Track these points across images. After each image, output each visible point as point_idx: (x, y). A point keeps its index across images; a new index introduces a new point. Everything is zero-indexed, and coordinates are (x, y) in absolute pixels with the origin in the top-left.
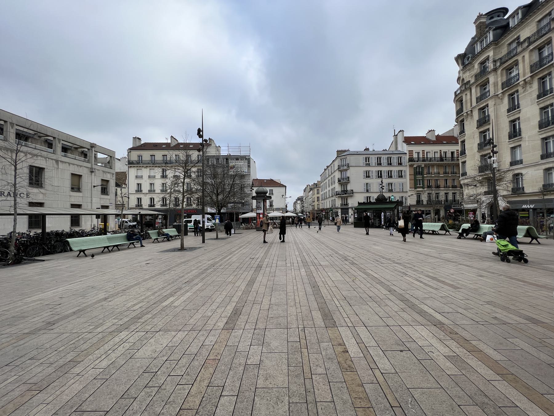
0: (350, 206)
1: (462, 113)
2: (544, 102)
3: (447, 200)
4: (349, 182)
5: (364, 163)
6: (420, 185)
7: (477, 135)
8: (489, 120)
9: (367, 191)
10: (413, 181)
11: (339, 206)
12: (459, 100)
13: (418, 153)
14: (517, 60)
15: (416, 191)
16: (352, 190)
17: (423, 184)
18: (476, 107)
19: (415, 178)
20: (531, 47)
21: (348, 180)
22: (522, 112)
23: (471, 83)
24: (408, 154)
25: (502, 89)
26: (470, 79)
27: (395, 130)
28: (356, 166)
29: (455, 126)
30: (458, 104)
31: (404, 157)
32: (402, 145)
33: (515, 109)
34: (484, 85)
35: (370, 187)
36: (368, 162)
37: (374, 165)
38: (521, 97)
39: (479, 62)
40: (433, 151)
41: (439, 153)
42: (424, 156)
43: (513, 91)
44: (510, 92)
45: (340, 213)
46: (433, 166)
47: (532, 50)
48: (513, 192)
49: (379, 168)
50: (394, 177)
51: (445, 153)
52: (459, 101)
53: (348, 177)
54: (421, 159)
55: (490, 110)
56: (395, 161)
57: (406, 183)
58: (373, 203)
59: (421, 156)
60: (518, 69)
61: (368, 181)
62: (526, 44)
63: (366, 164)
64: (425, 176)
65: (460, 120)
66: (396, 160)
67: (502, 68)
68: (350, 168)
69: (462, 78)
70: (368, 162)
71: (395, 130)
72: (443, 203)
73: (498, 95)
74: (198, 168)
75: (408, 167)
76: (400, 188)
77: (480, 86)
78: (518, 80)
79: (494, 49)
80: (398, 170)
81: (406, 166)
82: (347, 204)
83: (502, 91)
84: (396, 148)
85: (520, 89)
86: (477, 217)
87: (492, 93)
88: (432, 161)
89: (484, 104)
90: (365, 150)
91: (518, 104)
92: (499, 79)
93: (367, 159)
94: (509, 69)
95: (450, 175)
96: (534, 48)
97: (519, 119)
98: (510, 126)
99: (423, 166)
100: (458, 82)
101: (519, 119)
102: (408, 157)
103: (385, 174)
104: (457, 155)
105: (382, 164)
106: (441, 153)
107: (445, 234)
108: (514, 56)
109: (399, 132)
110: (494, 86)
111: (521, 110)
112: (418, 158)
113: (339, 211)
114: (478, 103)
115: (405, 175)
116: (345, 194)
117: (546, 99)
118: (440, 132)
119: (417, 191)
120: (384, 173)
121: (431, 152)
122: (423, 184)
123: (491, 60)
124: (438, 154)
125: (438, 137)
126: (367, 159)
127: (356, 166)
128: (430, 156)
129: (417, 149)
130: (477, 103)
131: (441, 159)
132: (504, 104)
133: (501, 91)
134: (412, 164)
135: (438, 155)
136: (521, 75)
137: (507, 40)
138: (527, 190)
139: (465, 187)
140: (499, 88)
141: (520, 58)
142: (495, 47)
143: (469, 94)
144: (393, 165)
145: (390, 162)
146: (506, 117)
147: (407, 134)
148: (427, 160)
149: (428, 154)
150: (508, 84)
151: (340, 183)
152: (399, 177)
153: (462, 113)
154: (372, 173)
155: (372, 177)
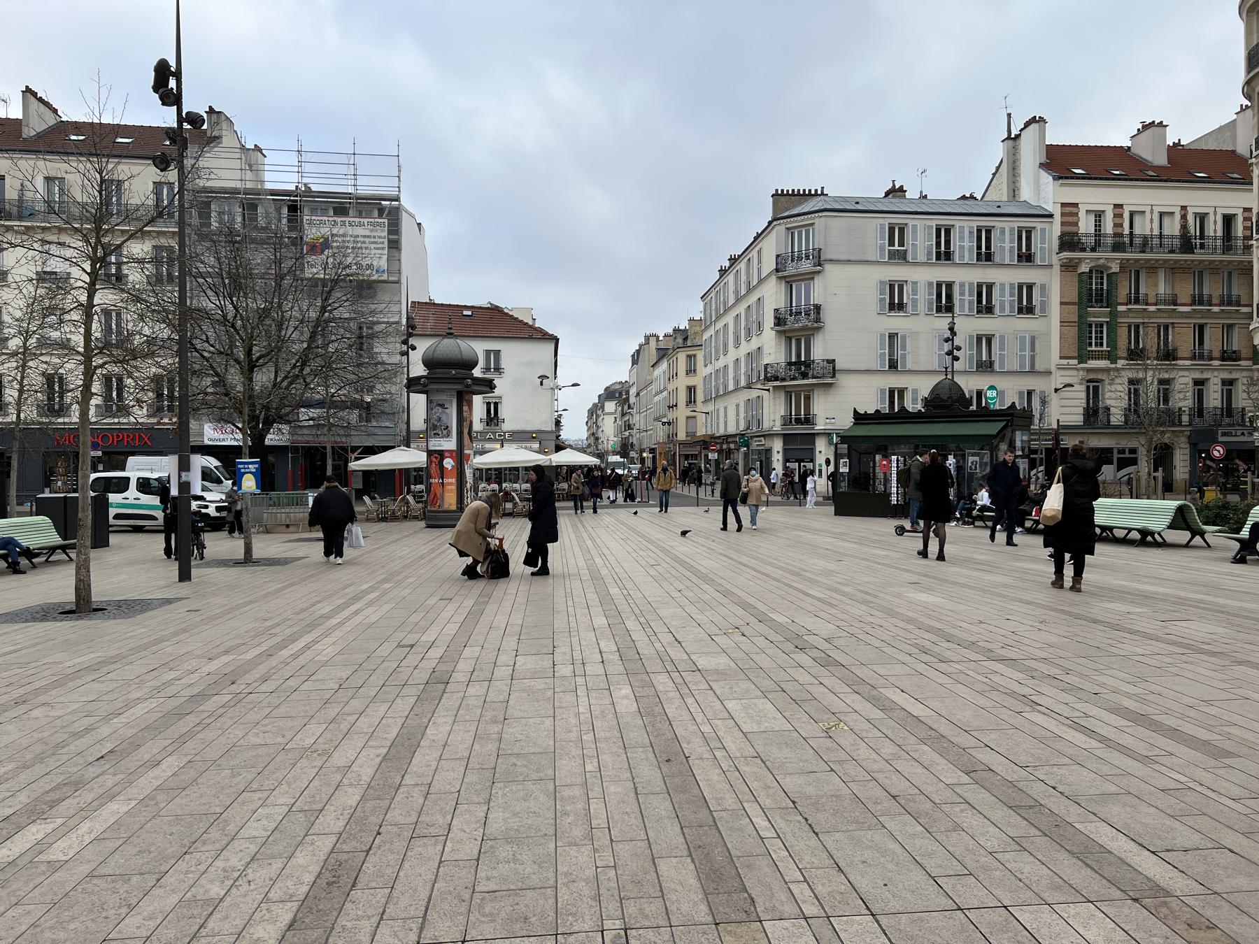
0: (820, 426)
3: (1199, 410)
4: (819, 329)
5: (882, 248)
6: (1102, 345)
9: (893, 365)
10: (1073, 332)
11: (777, 428)
13: (1099, 215)
15: (1083, 369)
19: (1080, 317)
21: (818, 320)
24: (1058, 218)
27: (1009, 115)
31: (1043, 230)
35: (904, 348)
36: (901, 244)
37: (921, 257)
41: (1178, 217)
42: (1119, 230)
45: (780, 457)
46: (1152, 268)
51: (1202, 218)
53: (818, 308)
54: (1110, 240)
57: (1048, 334)
59: (1108, 228)
61: (896, 323)
63: (892, 255)
64: (1121, 308)
66: (1012, 241)
68: (828, 267)
70: (901, 244)
71: (1009, 115)
72: (1185, 419)
81: (1050, 266)
82: (808, 420)
84: (1014, 191)
90: (887, 194)
93: (896, 234)
95: (1216, 309)
99: (1115, 268)
102: (1056, 229)
103: (967, 297)
104: (1245, 228)
105: (1038, 256)
106: (1184, 217)
107: (1187, 546)
109: (1027, 125)
112: (1098, 233)
113: (777, 446)
119: (1089, 370)
122: (1112, 342)
124: (1173, 222)
126: (896, 234)
128: (1144, 227)
134: (1071, 259)
135: (1173, 228)
144: (997, 259)
147: (1056, 136)
149: (1137, 219)
151: (784, 332)
152: (1020, 311)
154: (915, 292)
155: (915, 306)
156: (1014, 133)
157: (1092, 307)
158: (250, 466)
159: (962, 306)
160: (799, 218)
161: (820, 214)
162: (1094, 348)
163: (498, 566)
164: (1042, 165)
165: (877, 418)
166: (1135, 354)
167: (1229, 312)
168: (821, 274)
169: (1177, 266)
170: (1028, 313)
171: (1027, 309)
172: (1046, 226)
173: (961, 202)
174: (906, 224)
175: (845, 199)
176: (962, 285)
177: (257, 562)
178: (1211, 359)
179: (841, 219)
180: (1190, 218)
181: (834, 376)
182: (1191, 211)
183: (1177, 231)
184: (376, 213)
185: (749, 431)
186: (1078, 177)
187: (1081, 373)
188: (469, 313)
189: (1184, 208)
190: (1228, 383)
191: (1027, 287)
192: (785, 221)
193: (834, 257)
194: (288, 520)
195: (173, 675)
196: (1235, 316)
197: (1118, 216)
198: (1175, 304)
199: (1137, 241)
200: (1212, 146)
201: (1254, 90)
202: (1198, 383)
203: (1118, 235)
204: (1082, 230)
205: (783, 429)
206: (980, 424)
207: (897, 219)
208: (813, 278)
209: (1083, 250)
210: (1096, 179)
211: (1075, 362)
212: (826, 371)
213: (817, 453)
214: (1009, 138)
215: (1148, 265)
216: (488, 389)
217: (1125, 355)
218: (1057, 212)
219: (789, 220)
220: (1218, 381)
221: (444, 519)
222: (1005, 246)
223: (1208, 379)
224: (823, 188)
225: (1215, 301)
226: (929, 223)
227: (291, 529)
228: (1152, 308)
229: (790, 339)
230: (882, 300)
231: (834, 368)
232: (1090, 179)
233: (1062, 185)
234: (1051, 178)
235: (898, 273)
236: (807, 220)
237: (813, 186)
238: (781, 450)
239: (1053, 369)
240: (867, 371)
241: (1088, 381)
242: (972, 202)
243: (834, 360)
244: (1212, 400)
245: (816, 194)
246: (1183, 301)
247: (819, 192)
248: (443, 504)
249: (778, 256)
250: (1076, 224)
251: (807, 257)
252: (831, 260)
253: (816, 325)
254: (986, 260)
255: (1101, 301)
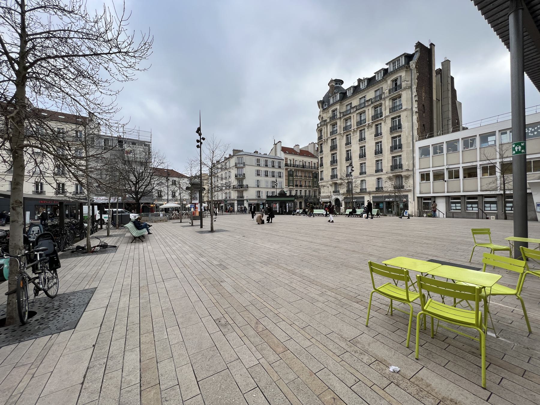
0: (245, 198)
7: (330, 156)
9: (258, 186)
11: (236, 198)
12: (320, 131)
13: (291, 160)
16: (248, 185)
17: (293, 183)
20: (357, 112)
23: (327, 122)
30: (319, 133)
34: (334, 125)
37: (263, 166)
40: (295, 160)
43: (348, 133)
45: (237, 204)
46: (299, 170)
47: (357, 114)
53: (244, 174)
54: (292, 165)
57: (283, 182)
59: (292, 163)
60: (350, 121)
61: (258, 178)
63: (258, 165)
74: (76, 147)
78: (351, 128)
79: (340, 105)
84: (276, 155)
85: (351, 133)
89: (334, 137)
90: (254, 152)
91: (350, 142)
92: (342, 124)
93: (258, 161)
98: (346, 154)
105: (282, 167)
106: (303, 162)
108: (349, 114)
109: (278, 142)
113: (236, 202)
116: (241, 187)
118: (302, 146)
119: (290, 188)
122: (293, 183)
123: (338, 110)
126: (258, 161)
128: (297, 163)
129: (290, 157)
130: (330, 135)
131: (303, 167)
132: (344, 140)
135: (301, 164)
137: (346, 103)
138: (385, 189)
143: (326, 128)
145: (267, 164)
147: (284, 145)
149: (296, 161)
150: (346, 128)
155: (262, 175)
163: (263, 222)
165: (271, 197)
175: (248, 153)
180: (313, 163)
184: (144, 145)
186: (287, 153)
195: (361, 222)
197: (293, 161)
202: (305, 191)
203: (293, 164)
207: (280, 161)
214: (275, 144)
222: (276, 165)
229: (238, 180)
237: (241, 149)
242: (266, 155)
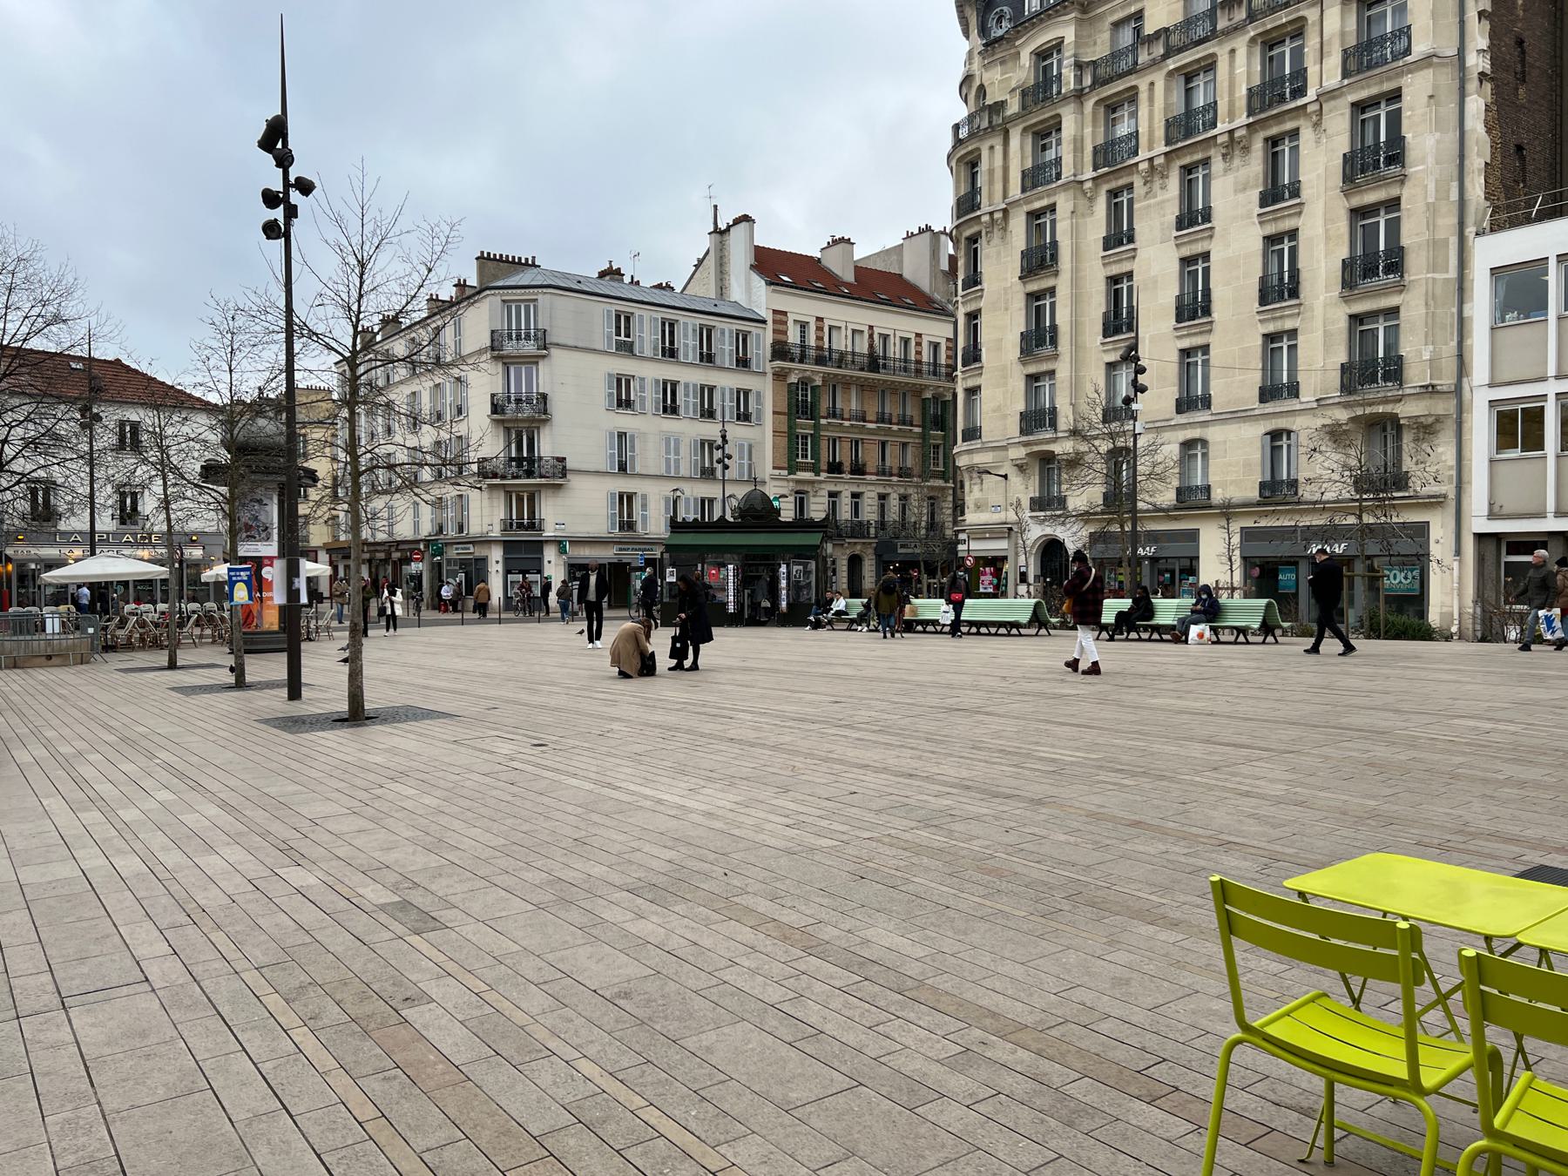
0: (549, 532)
1: (978, 213)
2: (1190, 242)
3: (882, 524)
4: (546, 421)
5: (610, 338)
6: (806, 457)
7: (1019, 303)
8: (1054, 257)
9: (622, 468)
10: (784, 442)
11: (496, 533)
12: (966, 162)
14: (1135, 88)
15: (793, 480)
16: (563, 460)
18: (1020, 205)
19: (790, 427)
20: (1172, 64)
21: (545, 412)
22: (1142, 254)
24: (770, 322)
25: (1095, 169)
26: (1008, 97)
27: (716, 207)
28: (576, 348)
29: (908, 237)
30: (964, 173)
31: (758, 336)
32: (748, 282)
33: (1121, 244)
34: (1044, 134)
35: (633, 450)
36: (628, 335)
37: (648, 352)
38: (1140, 209)
39: (1033, 46)
41: (866, 335)
42: (820, 343)
44: (1113, 185)
45: (500, 567)
46: (847, 383)
48: (1108, 507)
49: (669, 372)
50: (687, 411)
51: (885, 337)
52: (967, 163)
54: (813, 353)
55: (1059, 226)
56: (727, 348)
57: (762, 443)
58: (721, 526)
59: (812, 341)
60: (1134, 115)
62: (1159, 50)
64: (823, 421)
65: (968, 233)
66: (731, 345)
67: (1097, 98)
68: (554, 352)
69: (977, 83)
70: (628, 335)
71: (716, 207)
72: (872, 531)
73: (1082, 182)
75: (770, 377)
76: (668, 461)
77: (1034, 133)
80: (735, 387)
81: (764, 373)
82: (534, 525)
83: (1095, 174)
84: (722, 289)
85: (1138, 182)
86: (1006, 586)
87: (1067, 172)
88: (846, 368)
89: (1044, 202)
90: (602, 275)
91: (1131, 228)
92: (1088, 130)
94: (1111, 107)
95: (895, 427)
96: (1177, 69)
97: (1130, 275)
99: (819, 382)
100: (964, 91)
101: (1130, 275)
102: (769, 337)
103: (691, 399)
104: (948, 357)
105: (754, 361)
106: (871, 336)
107: (1036, 635)
108: (1129, 73)
109: (737, 221)
110: (1075, 150)
111: (1139, 251)
112: (803, 346)
113: (496, 555)
114: (1028, 194)
115: (759, 412)
117: (1193, 237)
119: (798, 482)
120: (687, 395)
121: (843, 328)
124: (862, 339)
125: (860, 271)
126: (623, 322)
127: (576, 348)
128: (841, 343)
129: (802, 307)
130: (1024, 190)
131: (874, 362)
133: (1089, 173)
134: (783, 368)
135: (862, 347)
136: (1143, 140)
139: (971, 479)
140: (1085, 160)
141: (1142, 83)
142: (1079, 16)
143: (999, 149)
144: (718, 361)
146: (1100, 262)
148: (830, 359)
149: (834, 333)
150: (1111, 155)
151: (502, 421)
152: (619, 405)
153: (978, 213)
154: (642, 389)
156: (722, 226)
157: (799, 418)
158: (242, 573)
159: (687, 407)
160: (519, 291)
161: (545, 290)
162: (800, 460)
163: (647, 667)
164: (752, 267)
166: (835, 468)
167: (905, 431)
168: (546, 359)
169: (866, 383)
170: (745, 421)
171: (744, 417)
172: (760, 331)
173: (656, 291)
174: (632, 313)
175: (565, 276)
176: (687, 386)
177: (249, 687)
178: (891, 475)
179: (562, 298)
180: (876, 337)
181: (564, 476)
182: (876, 331)
183: (866, 351)
185: (442, 537)
187: (791, 484)
188: (80, 366)
189: (871, 327)
190: (904, 498)
191: (709, 389)
192: (501, 291)
193: (561, 341)
194: (49, 650)
196: (908, 435)
197: (820, 329)
198: (865, 421)
199: (835, 356)
200: (880, 267)
201: (961, 234)
202: (832, 495)
204: (790, 340)
205: (503, 535)
206: (799, 535)
208: (537, 363)
209: (792, 360)
210: (802, 289)
211: (785, 472)
212: (556, 471)
213: (546, 563)
215: (843, 380)
216: (311, 482)
217: (825, 468)
218: (769, 318)
219: (505, 291)
220: (874, 495)
221: (270, 643)
222: (725, 348)
223: (863, 493)
224: (534, 258)
225: (894, 420)
226: (655, 315)
227: (55, 661)
228: (847, 423)
230: (610, 394)
231: (564, 467)
232: (796, 288)
233: (774, 291)
234: (763, 283)
235: (625, 366)
236: (530, 294)
237: (524, 254)
238: (500, 559)
239: (767, 479)
240: (597, 473)
241: (797, 492)
243: (565, 459)
244: (843, 513)
245: (526, 264)
246: (871, 418)
247: (530, 262)
248: (262, 623)
249: (493, 332)
250: (785, 333)
251: (528, 337)
252: (558, 345)
253: (544, 417)
254: (670, 357)
255: (806, 413)
